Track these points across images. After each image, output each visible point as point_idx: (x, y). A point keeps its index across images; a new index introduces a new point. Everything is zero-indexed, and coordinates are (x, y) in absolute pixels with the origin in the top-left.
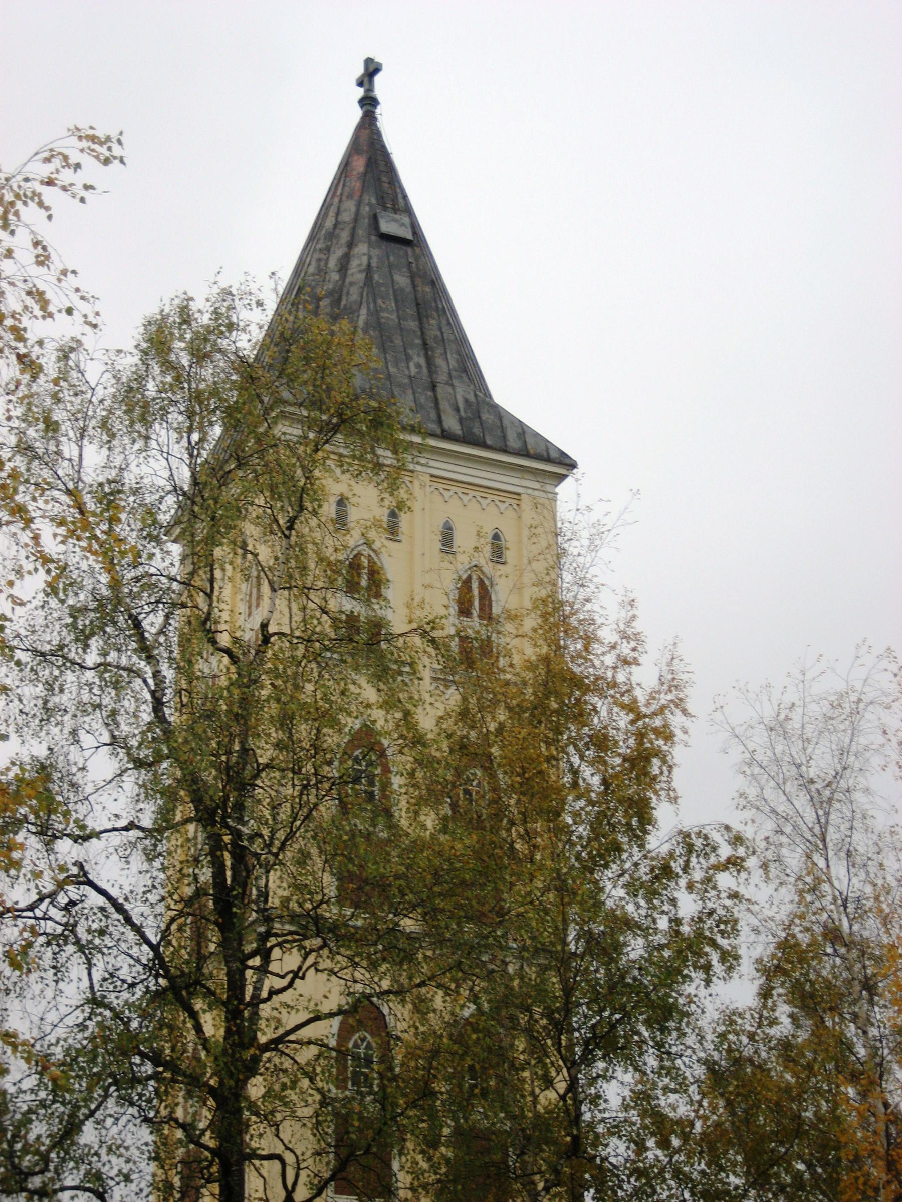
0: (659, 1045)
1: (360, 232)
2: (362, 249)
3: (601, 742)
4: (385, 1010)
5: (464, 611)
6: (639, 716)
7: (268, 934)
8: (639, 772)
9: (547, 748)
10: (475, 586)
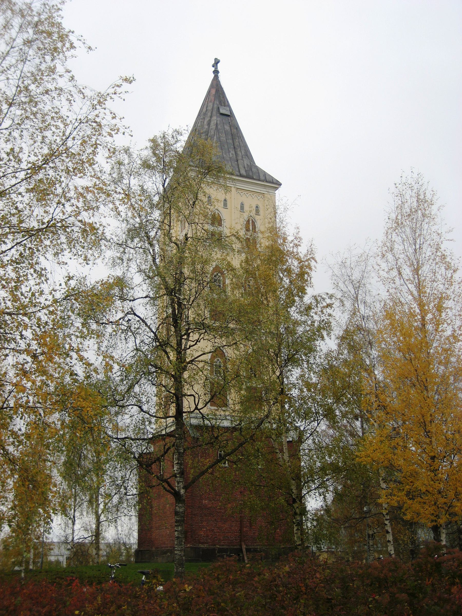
0: (308, 362)
1: (214, 113)
2: (214, 118)
3: (289, 271)
4: (225, 351)
5: (248, 230)
6: (301, 262)
7: (189, 329)
8: (302, 278)
9: (273, 270)
10: (251, 222)
